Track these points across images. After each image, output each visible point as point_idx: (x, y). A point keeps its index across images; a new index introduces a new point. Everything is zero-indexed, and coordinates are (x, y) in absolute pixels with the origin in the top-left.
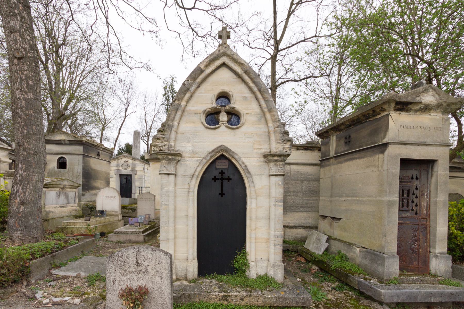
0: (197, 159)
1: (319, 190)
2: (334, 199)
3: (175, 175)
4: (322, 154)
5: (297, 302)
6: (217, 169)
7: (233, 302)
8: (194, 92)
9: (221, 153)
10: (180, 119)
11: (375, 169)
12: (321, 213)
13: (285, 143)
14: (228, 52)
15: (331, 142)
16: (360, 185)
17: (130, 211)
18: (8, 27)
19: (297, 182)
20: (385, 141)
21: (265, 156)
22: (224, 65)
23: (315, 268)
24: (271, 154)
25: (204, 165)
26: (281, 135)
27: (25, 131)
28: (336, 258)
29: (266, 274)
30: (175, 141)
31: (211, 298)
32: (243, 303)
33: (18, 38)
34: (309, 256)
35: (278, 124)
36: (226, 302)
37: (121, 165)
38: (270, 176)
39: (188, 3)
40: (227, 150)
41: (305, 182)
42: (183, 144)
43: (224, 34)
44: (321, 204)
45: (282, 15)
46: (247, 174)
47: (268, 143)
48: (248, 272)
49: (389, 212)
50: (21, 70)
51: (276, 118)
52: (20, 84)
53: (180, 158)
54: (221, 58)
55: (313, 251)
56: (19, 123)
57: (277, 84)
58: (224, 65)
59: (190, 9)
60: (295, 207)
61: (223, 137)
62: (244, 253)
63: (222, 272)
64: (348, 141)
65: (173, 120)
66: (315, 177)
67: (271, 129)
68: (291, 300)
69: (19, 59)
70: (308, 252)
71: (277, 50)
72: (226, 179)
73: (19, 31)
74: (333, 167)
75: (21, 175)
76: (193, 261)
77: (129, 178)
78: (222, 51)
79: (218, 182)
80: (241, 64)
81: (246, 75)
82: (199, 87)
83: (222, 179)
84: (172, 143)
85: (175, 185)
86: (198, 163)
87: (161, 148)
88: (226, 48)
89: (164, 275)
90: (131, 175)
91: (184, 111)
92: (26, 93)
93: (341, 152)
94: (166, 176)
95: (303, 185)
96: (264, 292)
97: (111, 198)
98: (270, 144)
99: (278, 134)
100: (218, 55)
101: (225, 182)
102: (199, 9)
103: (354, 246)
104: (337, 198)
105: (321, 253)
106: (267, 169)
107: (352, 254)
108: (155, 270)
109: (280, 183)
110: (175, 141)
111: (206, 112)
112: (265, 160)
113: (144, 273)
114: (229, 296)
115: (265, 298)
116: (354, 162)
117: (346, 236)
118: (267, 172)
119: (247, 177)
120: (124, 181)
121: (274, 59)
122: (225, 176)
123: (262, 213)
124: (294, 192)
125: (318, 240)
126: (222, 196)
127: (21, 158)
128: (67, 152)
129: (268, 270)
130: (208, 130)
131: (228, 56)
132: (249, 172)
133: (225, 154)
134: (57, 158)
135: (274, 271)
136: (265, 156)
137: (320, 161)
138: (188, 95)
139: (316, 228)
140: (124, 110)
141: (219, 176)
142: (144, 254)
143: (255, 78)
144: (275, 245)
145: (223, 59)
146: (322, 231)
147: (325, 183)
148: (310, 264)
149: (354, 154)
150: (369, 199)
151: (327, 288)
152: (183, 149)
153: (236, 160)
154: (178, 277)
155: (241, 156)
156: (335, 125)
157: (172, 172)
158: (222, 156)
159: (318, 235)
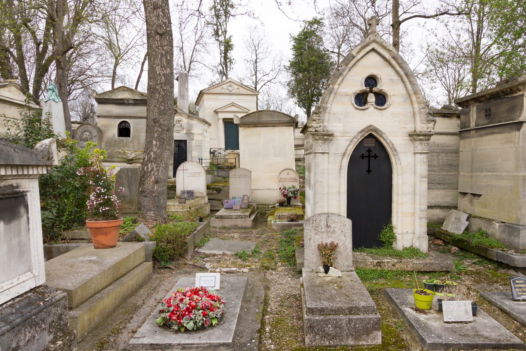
0: (347, 138)
2: (475, 174)
5: (442, 267)
6: (364, 147)
7: (386, 268)
11: (513, 145)
12: (461, 190)
14: (378, 40)
15: (471, 112)
16: (499, 160)
17: (215, 192)
18: (151, 3)
20: (521, 119)
21: (410, 135)
22: (373, 50)
23: (454, 249)
26: (426, 116)
27: (162, 107)
28: (477, 235)
29: (412, 246)
31: (366, 265)
32: (394, 269)
33: (161, 13)
34: (448, 237)
36: (379, 268)
38: (415, 153)
40: (376, 130)
44: (461, 180)
46: (394, 152)
48: (395, 244)
49: (523, 186)
50: (162, 46)
52: (161, 60)
54: (371, 45)
55: (452, 231)
56: (157, 99)
57: (401, 19)
58: (373, 50)
61: (371, 117)
62: (390, 227)
63: (369, 246)
64: (488, 114)
66: (453, 148)
67: (417, 110)
68: (436, 266)
69: (161, 35)
70: (446, 233)
72: (373, 157)
73: (161, 6)
74: (473, 140)
75: (155, 153)
77: (183, 145)
79: (366, 159)
83: (369, 157)
84: (326, 124)
86: (348, 142)
88: (376, 36)
89: (347, 234)
90: (185, 141)
92: (165, 68)
93: (481, 125)
94: (321, 155)
95: (440, 157)
96: (412, 260)
97: (194, 175)
98: (415, 123)
99: (422, 115)
103: (494, 222)
104: (478, 173)
105: (461, 233)
106: (412, 147)
107: (492, 230)
108: (341, 231)
109: (425, 160)
112: (411, 138)
113: (332, 233)
114: (382, 262)
115: (414, 263)
116: (494, 136)
117: (486, 213)
118: (412, 150)
119: (394, 155)
125: (458, 219)
126: (369, 173)
127: (156, 135)
128: (131, 115)
129: (414, 242)
130: (358, 110)
131: (377, 43)
132: (396, 150)
133: (373, 133)
134: (118, 123)
135: (420, 243)
136: (410, 135)
139: (456, 208)
141: (366, 154)
142: (332, 218)
144: (420, 218)
146: (462, 210)
147: (465, 156)
148: (449, 246)
149: (494, 128)
150: (508, 174)
151: (467, 264)
153: (384, 138)
156: (475, 96)
158: (371, 136)
159: (457, 214)
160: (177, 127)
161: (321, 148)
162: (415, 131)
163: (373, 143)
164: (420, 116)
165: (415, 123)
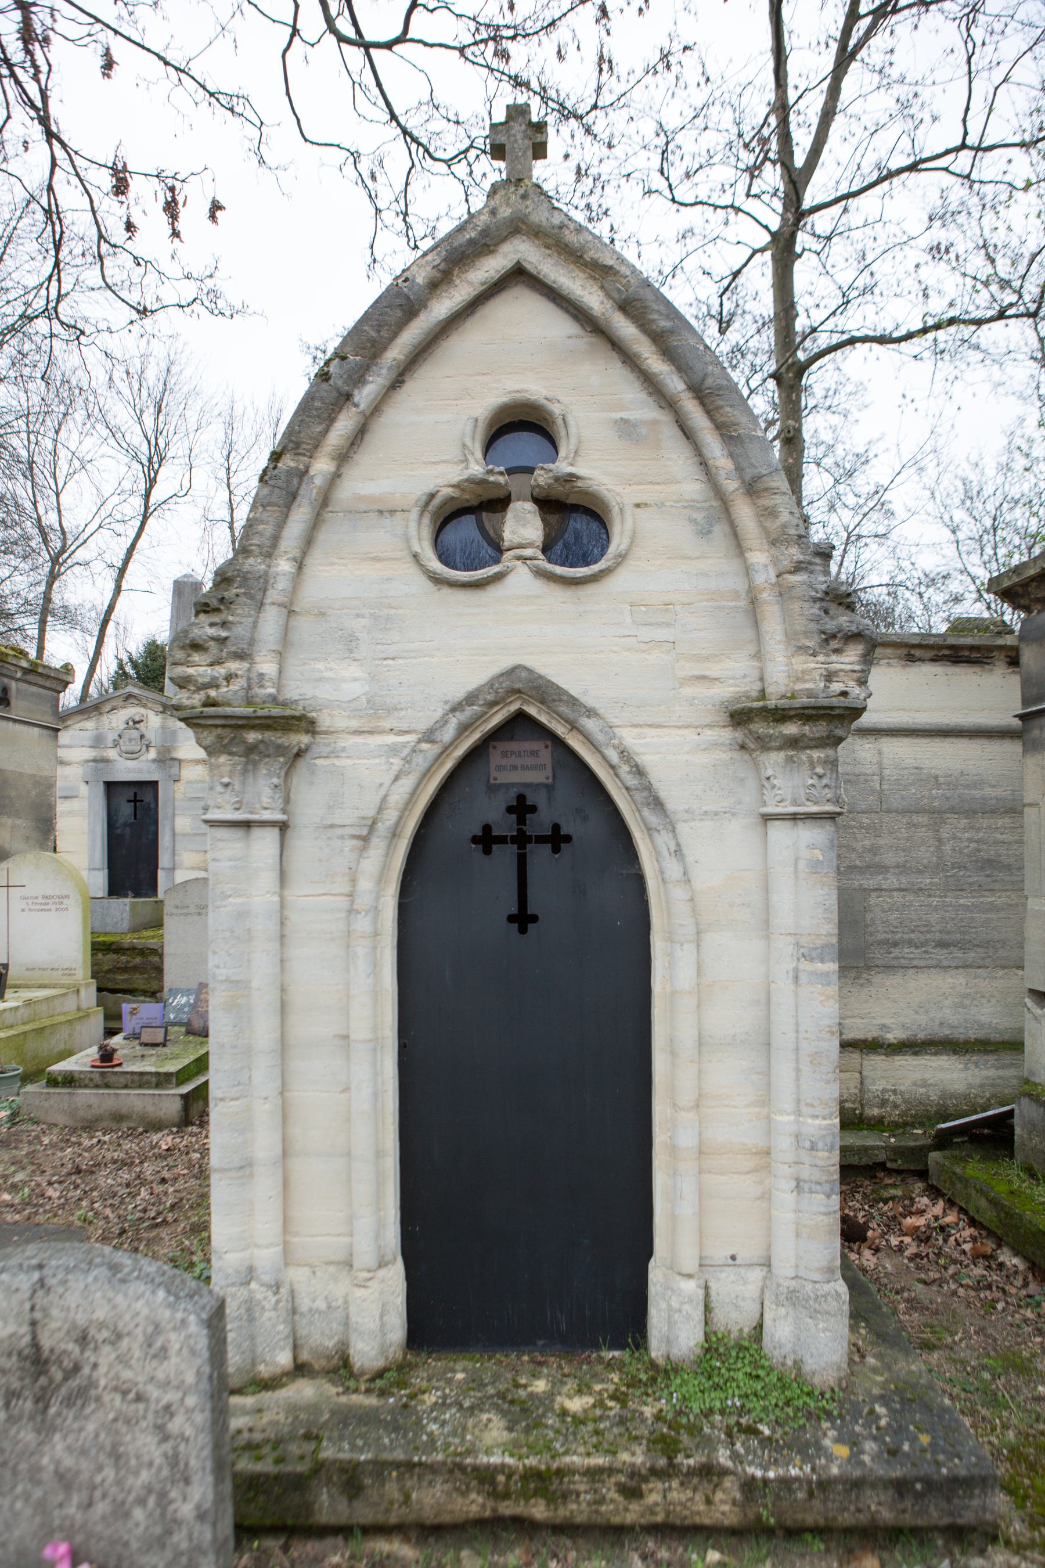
0: (391, 739)
1: (1021, 858)
3: (283, 827)
4: (1025, 684)
6: (493, 789)
8: (376, 409)
9: (514, 708)
10: (309, 541)
13: (836, 651)
14: (540, 216)
19: (916, 819)
21: (740, 717)
22: (519, 275)
24: (765, 709)
25: (427, 774)
26: (815, 610)
30: (281, 655)
35: (795, 553)
37: (111, 736)
38: (767, 818)
39: (379, 21)
40: (545, 691)
41: (952, 819)
42: (320, 666)
43: (517, 138)
45: (810, 64)
46: (646, 812)
47: (751, 649)
51: (784, 526)
53: (305, 739)
58: (519, 275)
59: (388, 46)
60: (911, 943)
61: (524, 625)
65: (269, 553)
66: (999, 792)
71: (796, 212)
72: (541, 840)
76: (382, 1273)
77: (148, 797)
78: (505, 212)
79: (505, 856)
80: (602, 272)
81: (628, 323)
82: (397, 383)
84: (267, 667)
85: (283, 877)
86: (397, 763)
87: (213, 693)
88: (524, 197)
90: (154, 784)
91: (325, 501)
94: (239, 833)
98: (758, 655)
99: (796, 606)
100: (485, 233)
101: (540, 856)
102: (426, 44)
106: (751, 784)
110: (281, 655)
111: (436, 502)
112: (739, 735)
119: (649, 829)
120: (126, 810)
121: (783, 249)
122: (540, 823)
123: (730, 1016)
124: (903, 869)
126: (523, 930)
130: (446, 591)
131: (537, 233)
132: (657, 804)
133: (532, 711)
136: (740, 717)
137: (1021, 717)
138: (344, 424)
140: (142, 486)
141: (505, 825)
143: (672, 332)
144: (799, 1186)
145: (515, 247)
152: (322, 693)
154: (305, 1356)
155: (615, 721)
157: (267, 816)
160: (130, 740)
161: (229, 797)
162: (763, 695)
163: (542, 767)
164: (785, 614)
165: (758, 655)
